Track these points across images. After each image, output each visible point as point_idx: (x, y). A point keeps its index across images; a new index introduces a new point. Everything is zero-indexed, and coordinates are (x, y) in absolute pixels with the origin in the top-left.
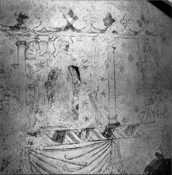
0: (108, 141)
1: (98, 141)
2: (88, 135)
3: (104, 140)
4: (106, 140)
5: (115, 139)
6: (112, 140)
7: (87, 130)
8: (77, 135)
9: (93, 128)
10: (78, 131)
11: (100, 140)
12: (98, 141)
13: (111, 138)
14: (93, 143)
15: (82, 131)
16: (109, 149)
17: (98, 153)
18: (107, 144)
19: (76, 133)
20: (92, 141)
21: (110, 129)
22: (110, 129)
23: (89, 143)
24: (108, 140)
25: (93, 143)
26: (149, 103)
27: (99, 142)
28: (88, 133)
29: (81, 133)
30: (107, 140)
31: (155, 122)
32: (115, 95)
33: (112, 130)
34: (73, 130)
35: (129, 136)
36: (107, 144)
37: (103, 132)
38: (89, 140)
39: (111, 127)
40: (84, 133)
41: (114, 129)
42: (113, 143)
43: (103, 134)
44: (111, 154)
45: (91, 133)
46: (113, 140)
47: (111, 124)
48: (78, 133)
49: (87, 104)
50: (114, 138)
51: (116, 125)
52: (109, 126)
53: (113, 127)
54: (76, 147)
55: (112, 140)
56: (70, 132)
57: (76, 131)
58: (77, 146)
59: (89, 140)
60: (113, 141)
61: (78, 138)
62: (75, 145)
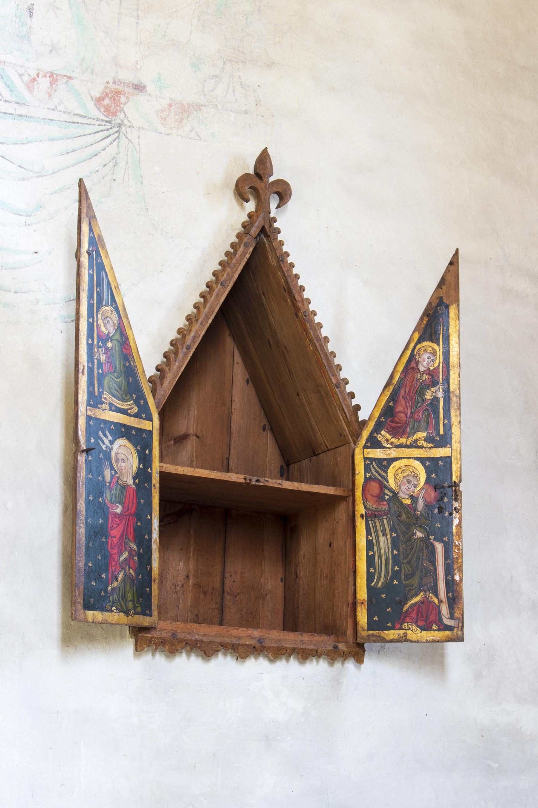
0: (108, 126)
1: (82, 116)
2: (55, 90)
3: (98, 120)
4: (102, 120)
5: (130, 127)
6: (120, 125)
7: (53, 78)
8: (23, 82)
9: (70, 78)
10: (26, 71)
11: (85, 117)
12: (82, 116)
13: (118, 121)
14: (66, 117)
15: (38, 75)
16: (112, 150)
17: (71, 120)
18: (106, 133)
19: (21, 75)
20: (64, 112)
21: (118, 93)
22: (118, 93)
23: (55, 115)
24: (110, 122)
25: (66, 117)
26: (233, 59)
27: (84, 120)
28: (54, 86)
29: (34, 80)
30: (107, 122)
31: (247, 114)
32: (138, 9)
33: (123, 99)
34: (14, 64)
35: (171, 129)
36: (106, 133)
37: (98, 95)
38: (56, 107)
39: (120, 88)
40: (44, 82)
41: (128, 98)
42: (122, 135)
43: (99, 101)
44: (114, 166)
45: (61, 84)
46: (123, 129)
47: (120, 82)
48: (26, 78)
49: (57, 8)
50: (126, 122)
51: (134, 88)
52: (114, 83)
53: (127, 89)
54: (17, 113)
55: (120, 125)
56: (5, 67)
57: (21, 70)
58: (21, 110)
59: (56, 107)
60: (125, 132)
61: (25, 92)
62: (17, 106)
